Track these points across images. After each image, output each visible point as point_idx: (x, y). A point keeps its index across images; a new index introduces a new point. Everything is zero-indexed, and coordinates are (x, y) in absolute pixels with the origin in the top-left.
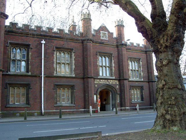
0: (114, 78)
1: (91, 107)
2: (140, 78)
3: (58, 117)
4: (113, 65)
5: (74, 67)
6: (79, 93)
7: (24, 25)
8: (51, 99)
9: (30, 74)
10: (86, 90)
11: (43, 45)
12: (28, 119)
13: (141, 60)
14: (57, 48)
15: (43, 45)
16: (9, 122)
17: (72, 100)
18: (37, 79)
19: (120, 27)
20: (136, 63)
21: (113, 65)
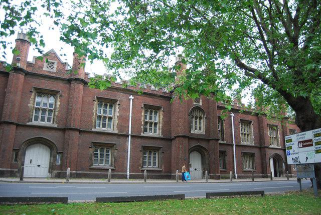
0: (280, 147)
1: (69, 169)
2: (278, 145)
3: (18, 180)
4: (279, 136)
5: (253, 137)
6: (257, 160)
7: (97, 76)
8: (240, 165)
9: (225, 142)
10: (263, 159)
11: (131, 101)
12: (255, 180)
13: (118, 103)
14: (36, 89)
15: (131, 101)
16: (53, 183)
17: (253, 166)
18: (231, 147)
19: (5, 30)
20: (58, 100)
21: (279, 136)
